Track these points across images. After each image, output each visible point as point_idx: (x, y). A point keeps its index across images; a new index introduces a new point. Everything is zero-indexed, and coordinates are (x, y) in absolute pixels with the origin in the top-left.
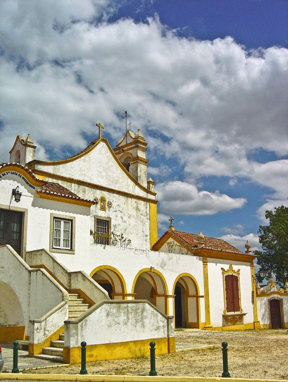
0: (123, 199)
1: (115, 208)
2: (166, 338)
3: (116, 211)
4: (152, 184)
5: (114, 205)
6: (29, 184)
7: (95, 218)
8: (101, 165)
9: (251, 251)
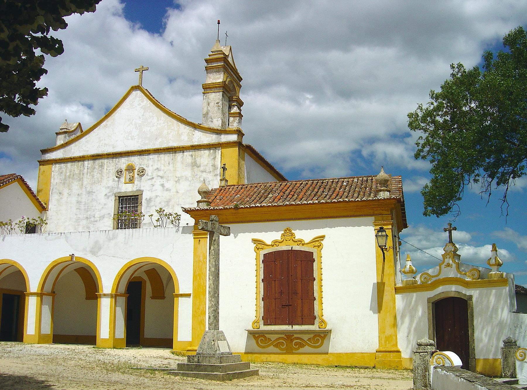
0: (165, 158)
1: (150, 174)
3: (153, 178)
4: (232, 117)
5: (149, 171)
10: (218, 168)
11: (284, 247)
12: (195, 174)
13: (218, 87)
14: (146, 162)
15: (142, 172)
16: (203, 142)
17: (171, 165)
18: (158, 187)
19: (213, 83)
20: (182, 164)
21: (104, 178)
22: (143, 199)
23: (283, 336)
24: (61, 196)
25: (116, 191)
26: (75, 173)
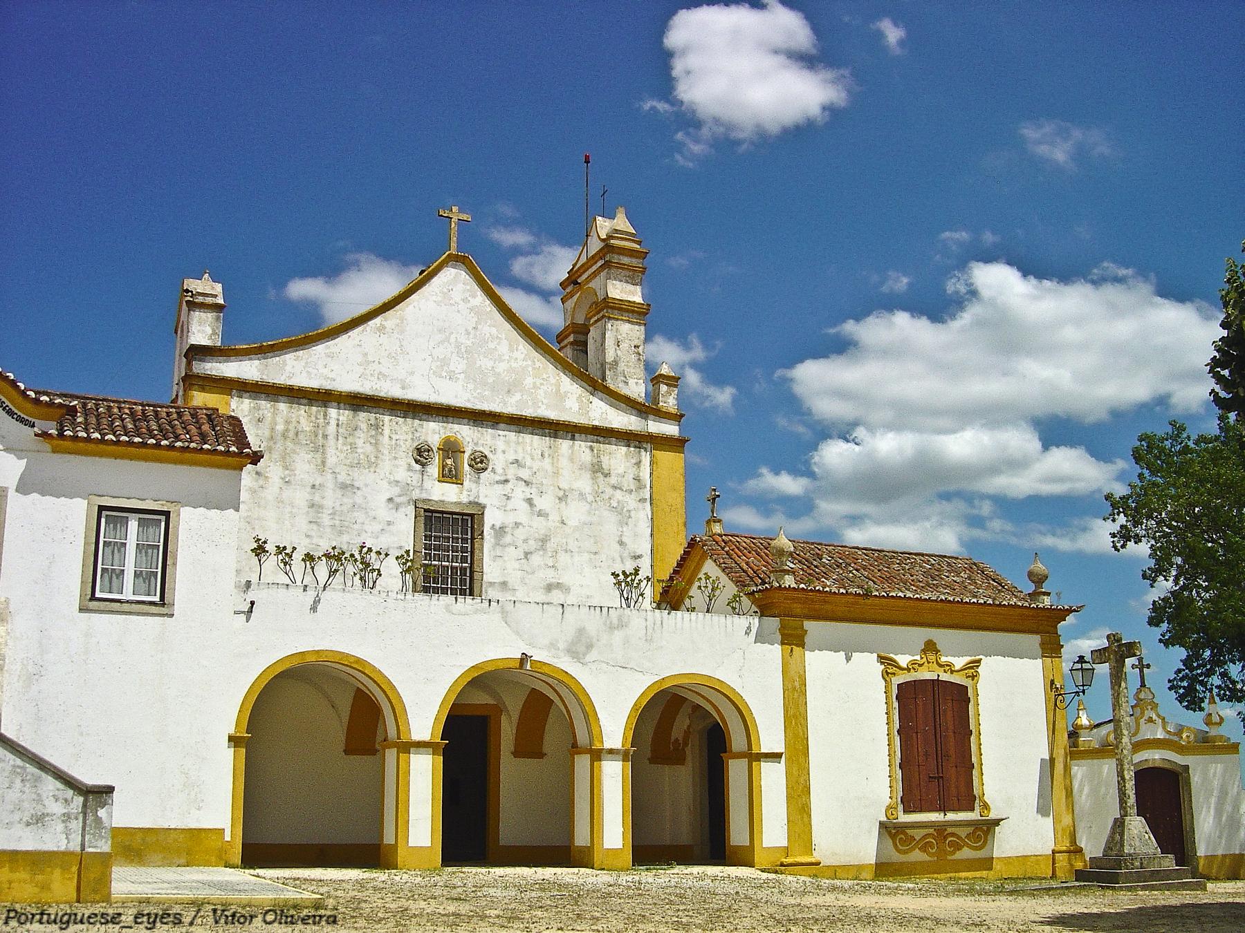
0: (534, 443)
1: (499, 471)
2: (72, 853)
3: (507, 481)
5: (498, 461)
6: (15, 416)
7: (416, 507)
8: (447, 340)
9: (1048, 594)
10: (645, 487)
11: (926, 674)
12: (600, 491)
13: (637, 312)
14: (500, 445)
15: (482, 462)
16: (610, 422)
17: (547, 460)
18: (518, 502)
19: (629, 301)
20: (573, 463)
21: (384, 457)
22: (485, 525)
23: (931, 831)
24: (261, 482)
25: (416, 494)
26: (300, 430)
